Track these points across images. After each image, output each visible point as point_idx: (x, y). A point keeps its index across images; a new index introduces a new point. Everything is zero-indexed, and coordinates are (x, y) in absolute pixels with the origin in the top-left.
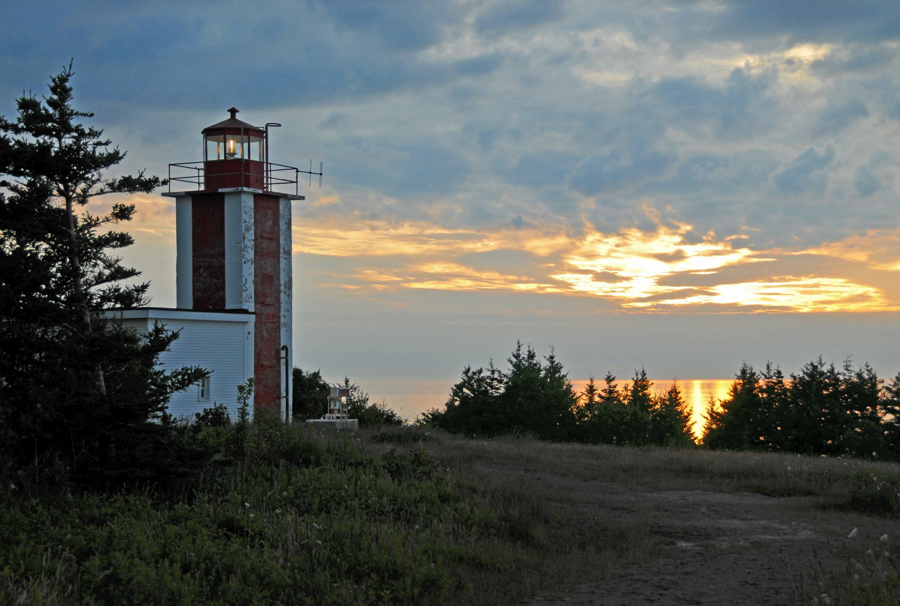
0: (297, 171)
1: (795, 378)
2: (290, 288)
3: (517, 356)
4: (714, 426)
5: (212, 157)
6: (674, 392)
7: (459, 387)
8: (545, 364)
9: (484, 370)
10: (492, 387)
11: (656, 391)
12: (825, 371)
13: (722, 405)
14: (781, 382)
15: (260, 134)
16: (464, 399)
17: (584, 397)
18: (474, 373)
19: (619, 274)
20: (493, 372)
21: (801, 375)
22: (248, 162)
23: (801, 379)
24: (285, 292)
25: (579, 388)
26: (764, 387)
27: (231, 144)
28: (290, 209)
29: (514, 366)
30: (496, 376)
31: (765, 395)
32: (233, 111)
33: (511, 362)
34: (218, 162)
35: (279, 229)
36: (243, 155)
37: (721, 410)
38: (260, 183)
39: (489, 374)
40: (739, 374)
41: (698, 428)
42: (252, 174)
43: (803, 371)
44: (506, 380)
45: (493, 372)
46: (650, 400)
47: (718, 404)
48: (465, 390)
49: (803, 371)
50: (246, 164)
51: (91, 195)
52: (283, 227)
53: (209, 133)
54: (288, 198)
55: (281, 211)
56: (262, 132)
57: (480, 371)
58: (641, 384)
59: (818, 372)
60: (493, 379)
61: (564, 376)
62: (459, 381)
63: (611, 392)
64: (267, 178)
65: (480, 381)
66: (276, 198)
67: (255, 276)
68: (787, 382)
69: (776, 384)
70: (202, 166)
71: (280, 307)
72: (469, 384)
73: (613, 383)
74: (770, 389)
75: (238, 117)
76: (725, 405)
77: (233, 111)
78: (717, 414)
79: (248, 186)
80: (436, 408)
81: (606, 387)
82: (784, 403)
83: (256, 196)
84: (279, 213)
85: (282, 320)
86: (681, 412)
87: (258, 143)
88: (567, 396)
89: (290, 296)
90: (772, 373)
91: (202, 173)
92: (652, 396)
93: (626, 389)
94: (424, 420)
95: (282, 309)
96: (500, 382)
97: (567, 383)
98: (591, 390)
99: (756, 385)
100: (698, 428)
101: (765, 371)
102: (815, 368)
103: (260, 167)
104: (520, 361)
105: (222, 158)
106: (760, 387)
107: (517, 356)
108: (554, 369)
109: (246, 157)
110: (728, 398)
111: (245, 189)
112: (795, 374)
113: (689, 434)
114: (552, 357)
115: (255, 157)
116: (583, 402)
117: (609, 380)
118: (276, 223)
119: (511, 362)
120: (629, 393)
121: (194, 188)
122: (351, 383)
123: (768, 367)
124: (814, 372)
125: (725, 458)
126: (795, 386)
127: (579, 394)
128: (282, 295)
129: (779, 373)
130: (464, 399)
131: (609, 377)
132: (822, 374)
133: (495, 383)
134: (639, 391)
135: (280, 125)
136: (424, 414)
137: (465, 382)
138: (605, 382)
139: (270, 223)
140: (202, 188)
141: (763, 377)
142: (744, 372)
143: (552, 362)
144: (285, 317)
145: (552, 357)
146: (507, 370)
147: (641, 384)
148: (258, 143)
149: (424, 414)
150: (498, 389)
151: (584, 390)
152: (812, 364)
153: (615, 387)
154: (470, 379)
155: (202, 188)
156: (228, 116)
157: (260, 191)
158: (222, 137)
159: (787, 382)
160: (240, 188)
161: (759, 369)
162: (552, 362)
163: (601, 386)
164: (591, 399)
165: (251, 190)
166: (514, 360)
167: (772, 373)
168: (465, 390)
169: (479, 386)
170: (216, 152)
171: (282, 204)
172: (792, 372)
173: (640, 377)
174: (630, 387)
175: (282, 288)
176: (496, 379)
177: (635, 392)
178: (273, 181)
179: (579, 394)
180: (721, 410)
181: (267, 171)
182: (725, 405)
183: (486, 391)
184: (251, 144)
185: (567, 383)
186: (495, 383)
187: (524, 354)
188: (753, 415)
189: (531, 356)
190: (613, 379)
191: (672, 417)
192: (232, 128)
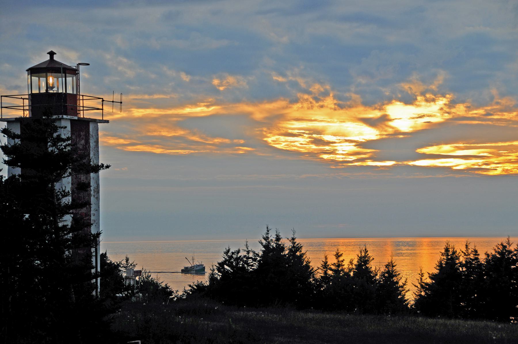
0: (103, 101)
1: (488, 255)
2: (98, 192)
3: (266, 239)
4: (423, 294)
5: (35, 91)
6: (390, 265)
7: (221, 265)
8: (287, 244)
9: (241, 251)
10: (248, 265)
11: (378, 267)
12: (513, 250)
13: (430, 277)
14: (477, 259)
15: (74, 72)
16: (225, 274)
17: (320, 271)
18: (233, 253)
19: (337, 152)
20: (248, 252)
21: (494, 253)
22: (66, 94)
23: (494, 257)
24: (94, 196)
25: (315, 264)
26: (464, 262)
27: (51, 80)
28: (98, 130)
29: (264, 247)
30: (251, 255)
31: (464, 269)
32: (52, 54)
33: (262, 243)
34: (40, 95)
35: (89, 146)
37: (429, 281)
38: (75, 111)
39: (245, 253)
40: (443, 251)
41: (410, 297)
42: (69, 104)
43: (495, 250)
44: (259, 259)
45: (248, 252)
46: (371, 272)
47: (426, 276)
48: (226, 267)
49: (495, 250)
50: (63, 97)
51: (64, 177)
52: (92, 144)
53: (34, 71)
54: (95, 121)
55: (91, 133)
57: (238, 252)
58: (364, 261)
59: (506, 251)
60: (248, 258)
61: (303, 254)
62: (221, 260)
63: (339, 266)
65: (238, 259)
66: (86, 122)
67: (72, 184)
68: (482, 258)
69: (473, 260)
71: (90, 208)
72: (229, 262)
73: (341, 259)
74: (468, 264)
75: (56, 58)
76: (433, 277)
77: (52, 54)
78: (427, 284)
79: (66, 114)
80: (200, 281)
81: (336, 261)
82: (480, 276)
83: (72, 121)
84: (89, 134)
85: (92, 218)
86: (397, 283)
87: (71, 78)
88: (307, 271)
89: (98, 198)
90: (470, 251)
91: (27, 102)
92: (373, 269)
93: (351, 263)
94: (191, 290)
95: (92, 209)
96: (254, 260)
97: (306, 259)
98: (325, 266)
99: (457, 261)
100: (410, 297)
101: (464, 250)
102: (504, 247)
103: (74, 98)
104: (269, 242)
105: (43, 91)
106: (460, 263)
107: (266, 239)
108: (295, 249)
110: (436, 272)
111: (65, 116)
112: (489, 253)
113: (403, 300)
114: (293, 239)
116: (319, 274)
117: (338, 256)
118: (87, 142)
119: (262, 243)
120: (354, 267)
121: (19, 114)
122: (130, 262)
123: (467, 246)
124: (504, 252)
125: (438, 324)
126: (488, 261)
127: (315, 269)
128: (92, 198)
129: (476, 251)
130: (225, 274)
131: (337, 254)
132: (510, 252)
133: (250, 261)
134: (363, 265)
135: (88, 64)
136: (190, 286)
137: (226, 260)
138: (334, 257)
139: (83, 142)
140: (27, 114)
141: (463, 254)
142: (447, 250)
143: (294, 243)
144: (94, 215)
145: (293, 239)
146: (260, 250)
147: (364, 261)
148: (71, 78)
149: (190, 286)
150: (252, 266)
151: (320, 266)
152: (502, 245)
153: (342, 261)
154: (231, 257)
155: (27, 114)
156: (48, 58)
157: (76, 118)
158: (45, 74)
159: (482, 258)
160: (61, 116)
161: (460, 248)
162: (294, 243)
163: (332, 260)
164: (326, 273)
165: (69, 117)
166: (264, 242)
167: (470, 251)
168: (226, 267)
169: (237, 264)
170: (40, 85)
171: (92, 126)
172: (486, 250)
173: (363, 254)
174: (355, 262)
175: (92, 193)
176: (251, 258)
177: (359, 266)
179: (315, 269)
180: (429, 281)
182: (433, 277)
183: (243, 267)
184: (67, 78)
185: (306, 259)
186: (250, 261)
187: (272, 237)
188: (453, 284)
189: (278, 239)
190: (341, 255)
191: (390, 286)
192: (52, 67)
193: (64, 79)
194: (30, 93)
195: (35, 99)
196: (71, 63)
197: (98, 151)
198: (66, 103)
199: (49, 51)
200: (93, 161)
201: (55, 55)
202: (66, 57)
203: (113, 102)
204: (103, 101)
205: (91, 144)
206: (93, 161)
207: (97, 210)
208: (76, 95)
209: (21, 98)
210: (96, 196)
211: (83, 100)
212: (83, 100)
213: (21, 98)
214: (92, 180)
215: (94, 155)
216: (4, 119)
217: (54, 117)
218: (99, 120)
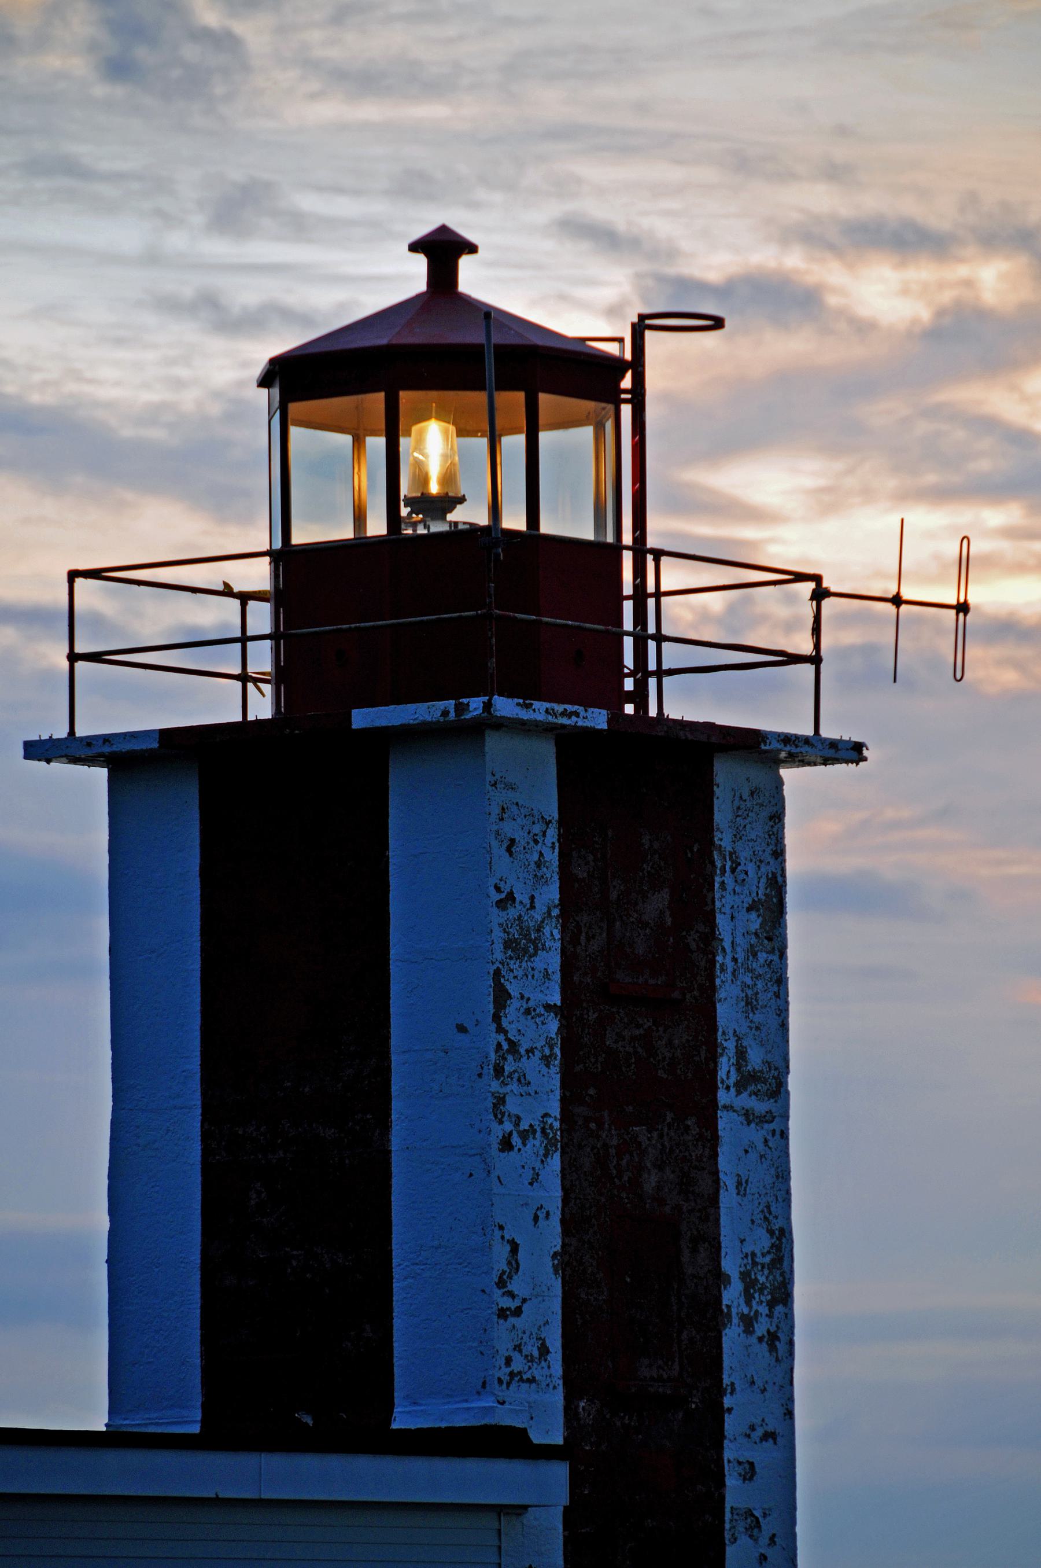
0: (820, 594)
5: (317, 527)
15: (594, 379)
24: (748, 1323)
32: (443, 250)
35: (710, 937)
36: (495, 510)
56: (615, 366)
64: (640, 595)
70: (258, 575)
75: (472, 278)
77: (443, 250)
79: (526, 691)
83: (571, 744)
84: (708, 844)
87: (587, 433)
105: (377, 526)
109: (515, 520)
111: (505, 707)
115: (568, 519)
118: (695, 908)
139: (657, 904)
155: (262, 706)
156: (413, 276)
157: (598, 719)
160: (476, 705)
165: (539, 711)
175: (732, 1296)
178: (673, 655)
181: (640, 595)
184: (545, 438)
193: (514, 444)
194: (278, 545)
195: (315, 591)
196: (583, 312)
197: (781, 981)
198: (546, 612)
199: (421, 230)
200: (741, 1054)
201: (466, 265)
202: (540, 283)
203: (897, 600)
204: (820, 594)
205: (722, 922)
206: (741, 1054)
207: (770, 1436)
208: (601, 557)
209: (227, 592)
210: (761, 1328)
211: (244, 639)
212: (244, 639)
213: (227, 592)
214: (728, 1199)
215: (750, 1004)
216: (89, 741)
217: (610, 833)
218: (787, 739)
